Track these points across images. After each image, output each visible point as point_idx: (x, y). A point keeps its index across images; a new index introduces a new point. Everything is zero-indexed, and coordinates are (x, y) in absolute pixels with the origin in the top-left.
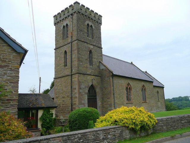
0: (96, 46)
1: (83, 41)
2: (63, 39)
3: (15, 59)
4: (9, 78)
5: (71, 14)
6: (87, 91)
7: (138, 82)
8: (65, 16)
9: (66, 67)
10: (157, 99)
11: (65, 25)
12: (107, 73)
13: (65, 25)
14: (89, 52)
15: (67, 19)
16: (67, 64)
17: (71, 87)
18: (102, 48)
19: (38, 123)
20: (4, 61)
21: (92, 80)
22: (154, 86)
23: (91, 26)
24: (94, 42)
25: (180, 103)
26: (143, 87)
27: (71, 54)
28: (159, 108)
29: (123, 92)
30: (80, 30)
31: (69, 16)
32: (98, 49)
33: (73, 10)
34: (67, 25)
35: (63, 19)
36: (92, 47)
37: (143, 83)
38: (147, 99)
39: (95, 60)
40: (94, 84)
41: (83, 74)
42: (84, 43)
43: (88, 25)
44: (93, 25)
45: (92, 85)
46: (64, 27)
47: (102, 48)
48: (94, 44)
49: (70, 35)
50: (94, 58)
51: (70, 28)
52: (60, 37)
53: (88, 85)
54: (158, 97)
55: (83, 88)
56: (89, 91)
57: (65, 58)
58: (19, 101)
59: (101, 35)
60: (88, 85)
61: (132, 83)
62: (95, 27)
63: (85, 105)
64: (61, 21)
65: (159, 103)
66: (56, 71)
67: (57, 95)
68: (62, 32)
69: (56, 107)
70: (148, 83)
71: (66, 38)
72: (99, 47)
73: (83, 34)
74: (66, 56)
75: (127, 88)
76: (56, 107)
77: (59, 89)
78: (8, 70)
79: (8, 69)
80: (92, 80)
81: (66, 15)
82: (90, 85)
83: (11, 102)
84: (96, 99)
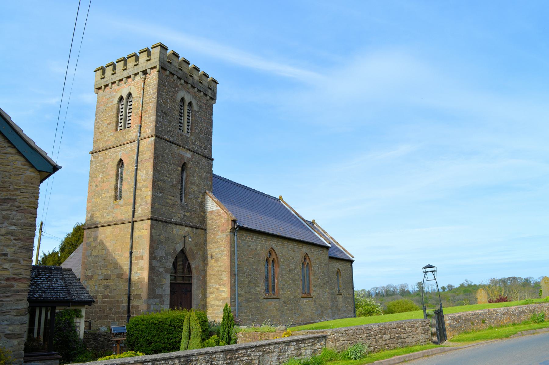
0: (198, 154)
1: (167, 138)
2: (117, 130)
3: (30, 185)
4: (13, 228)
5: (143, 72)
6: (170, 265)
7: (293, 246)
8: (126, 74)
9: (121, 202)
10: (336, 289)
11: (125, 97)
12: (223, 220)
13: (125, 97)
14: (180, 169)
15: (130, 80)
16: (123, 194)
17: (131, 253)
18: (213, 160)
19: (44, 338)
20: (4, 189)
21: (184, 237)
22: (330, 258)
23: (190, 104)
24: (193, 143)
25: (390, 302)
26: (305, 259)
27: (137, 169)
28: (340, 310)
29: (257, 270)
30: (162, 111)
31: (136, 74)
32: (204, 160)
33: (149, 62)
34: (130, 95)
35: (121, 80)
36: (188, 155)
37: (305, 249)
38: (312, 288)
39: (195, 188)
40: (188, 248)
41: (162, 222)
42: (169, 143)
43: (183, 100)
44: (194, 103)
45: (183, 251)
46: (121, 98)
47: (213, 160)
48: (195, 148)
49: (134, 122)
50: (193, 183)
51: (136, 103)
52: (109, 124)
53: (175, 250)
54: (338, 286)
55: (162, 257)
56: (175, 264)
57: (119, 177)
58: (33, 282)
59: (212, 127)
60: (175, 250)
61: (279, 247)
62: (200, 106)
63: (163, 301)
64: (113, 83)
65: (340, 299)
66: (90, 208)
67: (89, 273)
68: (115, 110)
69: (89, 303)
70: (316, 251)
71: (125, 127)
72: (205, 157)
73: (170, 122)
74: (122, 173)
75: (267, 260)
76: (89, 303)
77: (96, 256)
78: (11, 210)
79: (11, 208)
80: (184, 237)
81: (131, 70)
82: (179, 249)
83: (16, 284)
84: (191, 284)
